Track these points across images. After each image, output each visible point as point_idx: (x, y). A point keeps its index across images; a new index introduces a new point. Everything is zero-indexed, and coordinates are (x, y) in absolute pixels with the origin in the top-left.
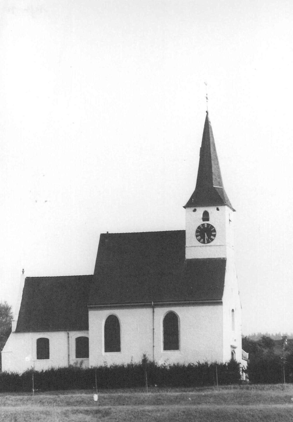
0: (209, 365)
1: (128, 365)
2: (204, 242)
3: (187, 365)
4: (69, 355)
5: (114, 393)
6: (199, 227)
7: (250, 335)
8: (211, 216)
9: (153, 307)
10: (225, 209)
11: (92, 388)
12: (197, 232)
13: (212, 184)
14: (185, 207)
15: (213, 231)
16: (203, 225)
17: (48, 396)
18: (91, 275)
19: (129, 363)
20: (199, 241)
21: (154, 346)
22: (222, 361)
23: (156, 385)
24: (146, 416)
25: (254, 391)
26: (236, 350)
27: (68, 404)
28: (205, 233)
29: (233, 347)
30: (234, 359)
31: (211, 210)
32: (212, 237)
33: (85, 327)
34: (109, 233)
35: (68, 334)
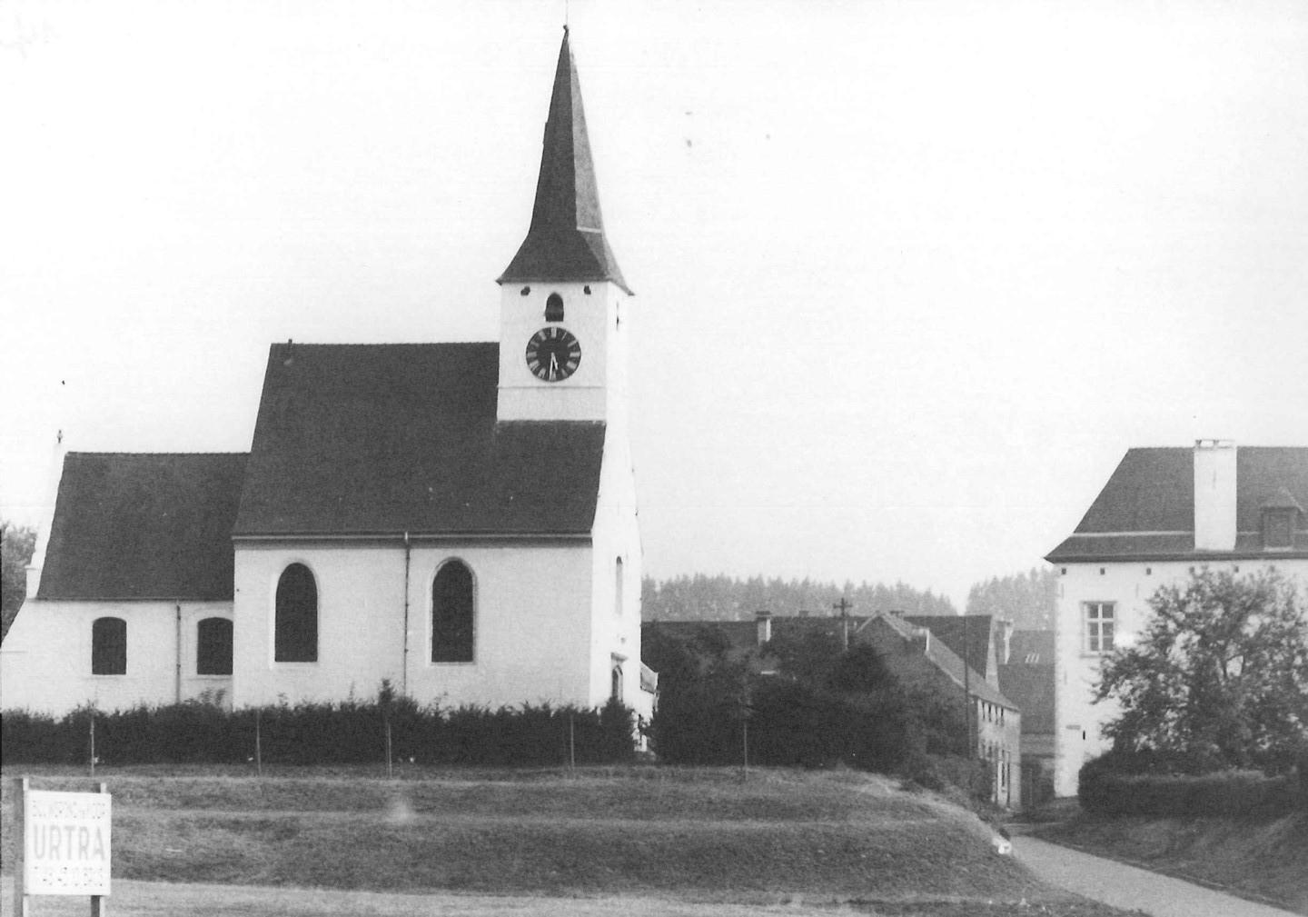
0: (553, 713)
1: (343, 706)
2: (546, 378)
3: (494, 710)
4: (179, 666)
5: (305, 776)
6: (536, 337)
7: (670, 580)
8: (567, 308)
9: (407, 546)
10: (606, 293)
11: (244, 761)
12: (530, 348)
13: (575, 224)
14: (500, 282)
15: (572, 347)
16: (547, 331)
17: (133, 779)
20: (536, 372)
21: (406, 651)
22: (587, 702)
23: (412, 760)
24: (390, 843)
25: (665, 783)
26: (625, 667)
27: (188, 803)
28: (553, 354)
29: (617, 659)
30: (619, 698)
31: (571, 293)
32: (570, 365)
33: (225, 591)
35: (178, 609)
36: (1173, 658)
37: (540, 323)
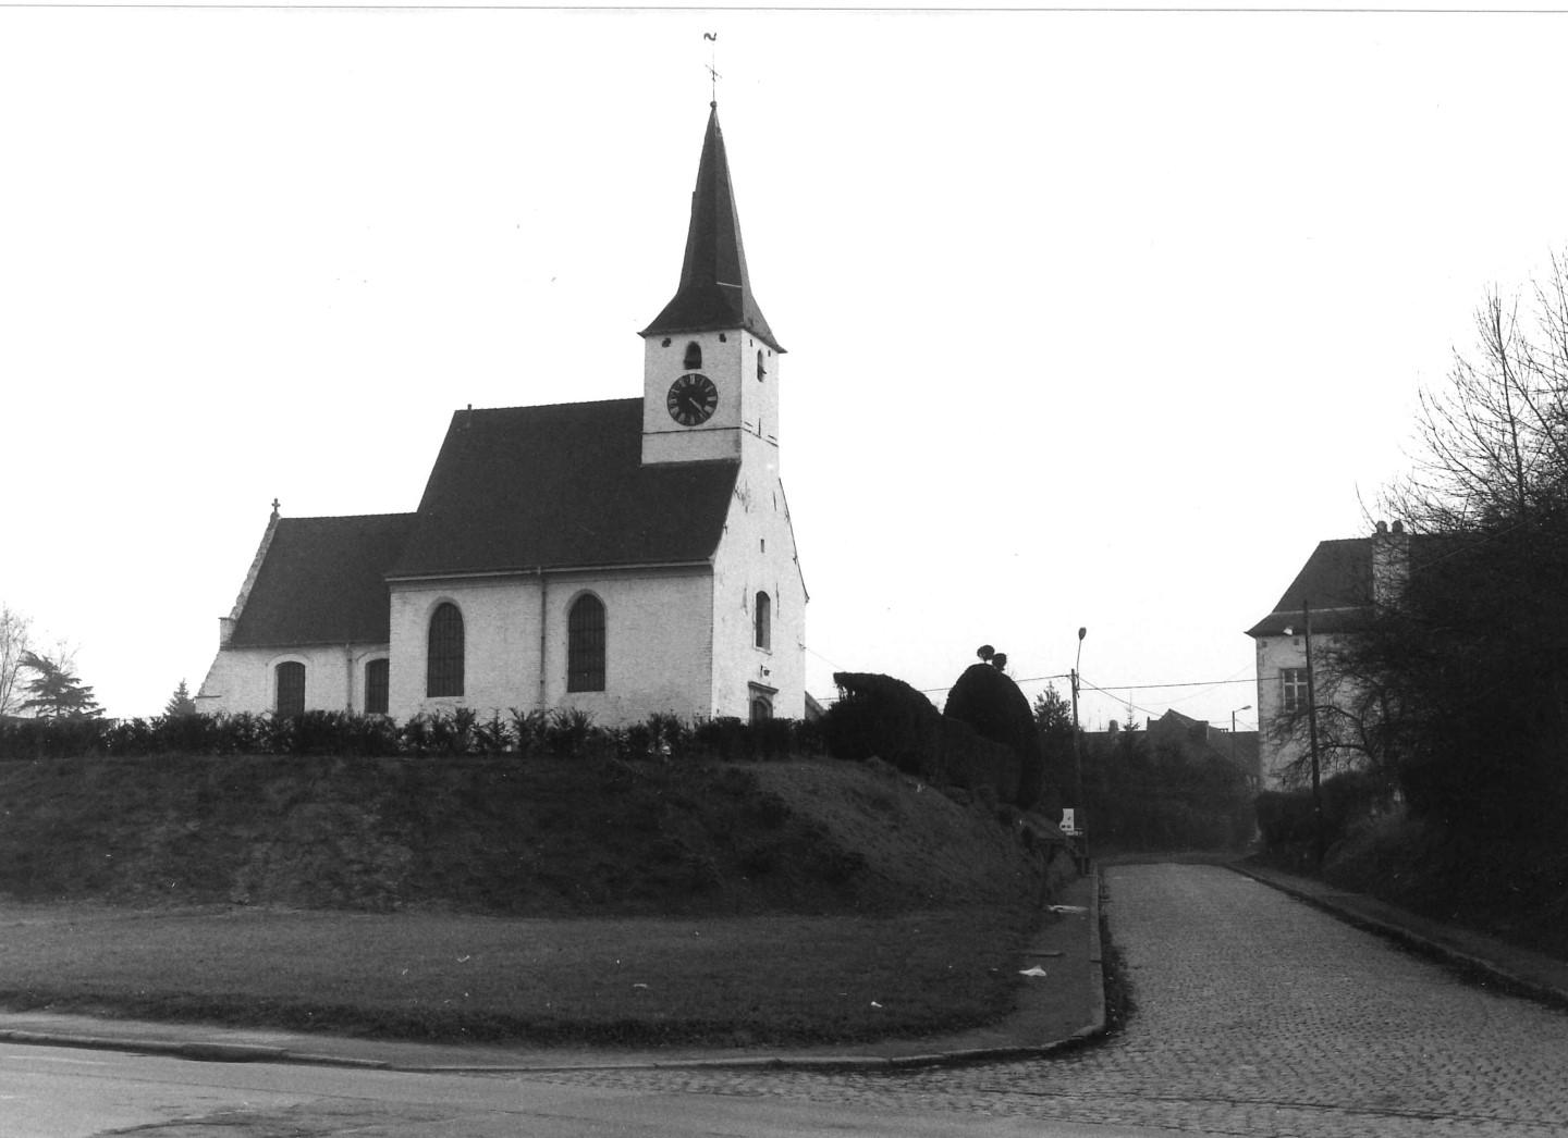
8: (705, 356)
14: (643, 334)
15: (709, 392)
16: (686, 378)
18: (412, 514)
19: (526, 708)
31: (709, 343)
33: (381, 636)
34: (473, 408)
36: (230, 716)
37: (679, 372)
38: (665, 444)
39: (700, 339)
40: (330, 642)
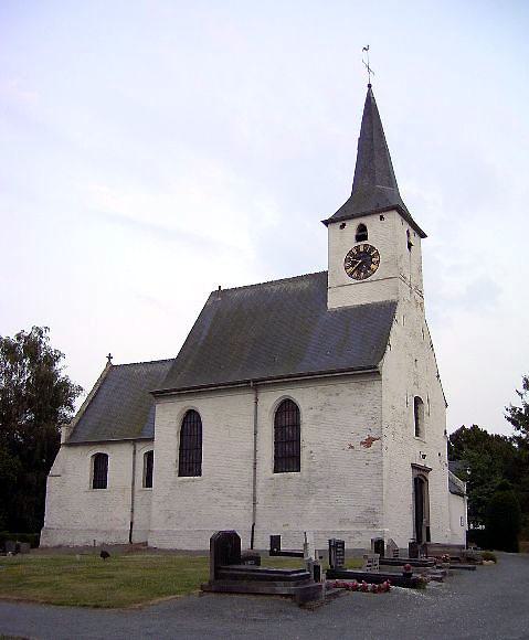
31: (372, 223)
38: (346, 295)
39: (365, 221)
40: (458, 551)
